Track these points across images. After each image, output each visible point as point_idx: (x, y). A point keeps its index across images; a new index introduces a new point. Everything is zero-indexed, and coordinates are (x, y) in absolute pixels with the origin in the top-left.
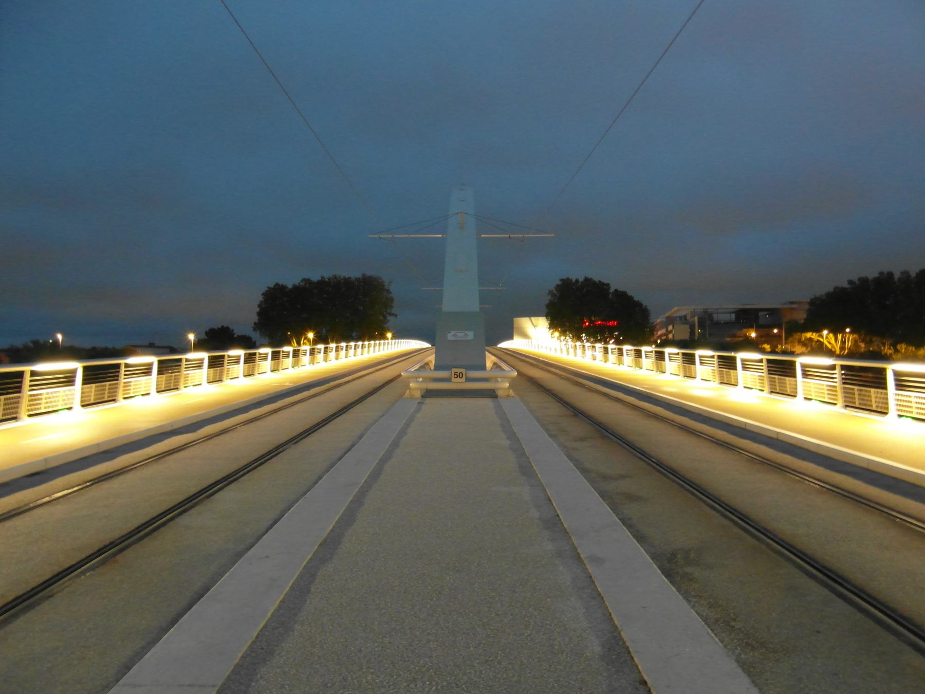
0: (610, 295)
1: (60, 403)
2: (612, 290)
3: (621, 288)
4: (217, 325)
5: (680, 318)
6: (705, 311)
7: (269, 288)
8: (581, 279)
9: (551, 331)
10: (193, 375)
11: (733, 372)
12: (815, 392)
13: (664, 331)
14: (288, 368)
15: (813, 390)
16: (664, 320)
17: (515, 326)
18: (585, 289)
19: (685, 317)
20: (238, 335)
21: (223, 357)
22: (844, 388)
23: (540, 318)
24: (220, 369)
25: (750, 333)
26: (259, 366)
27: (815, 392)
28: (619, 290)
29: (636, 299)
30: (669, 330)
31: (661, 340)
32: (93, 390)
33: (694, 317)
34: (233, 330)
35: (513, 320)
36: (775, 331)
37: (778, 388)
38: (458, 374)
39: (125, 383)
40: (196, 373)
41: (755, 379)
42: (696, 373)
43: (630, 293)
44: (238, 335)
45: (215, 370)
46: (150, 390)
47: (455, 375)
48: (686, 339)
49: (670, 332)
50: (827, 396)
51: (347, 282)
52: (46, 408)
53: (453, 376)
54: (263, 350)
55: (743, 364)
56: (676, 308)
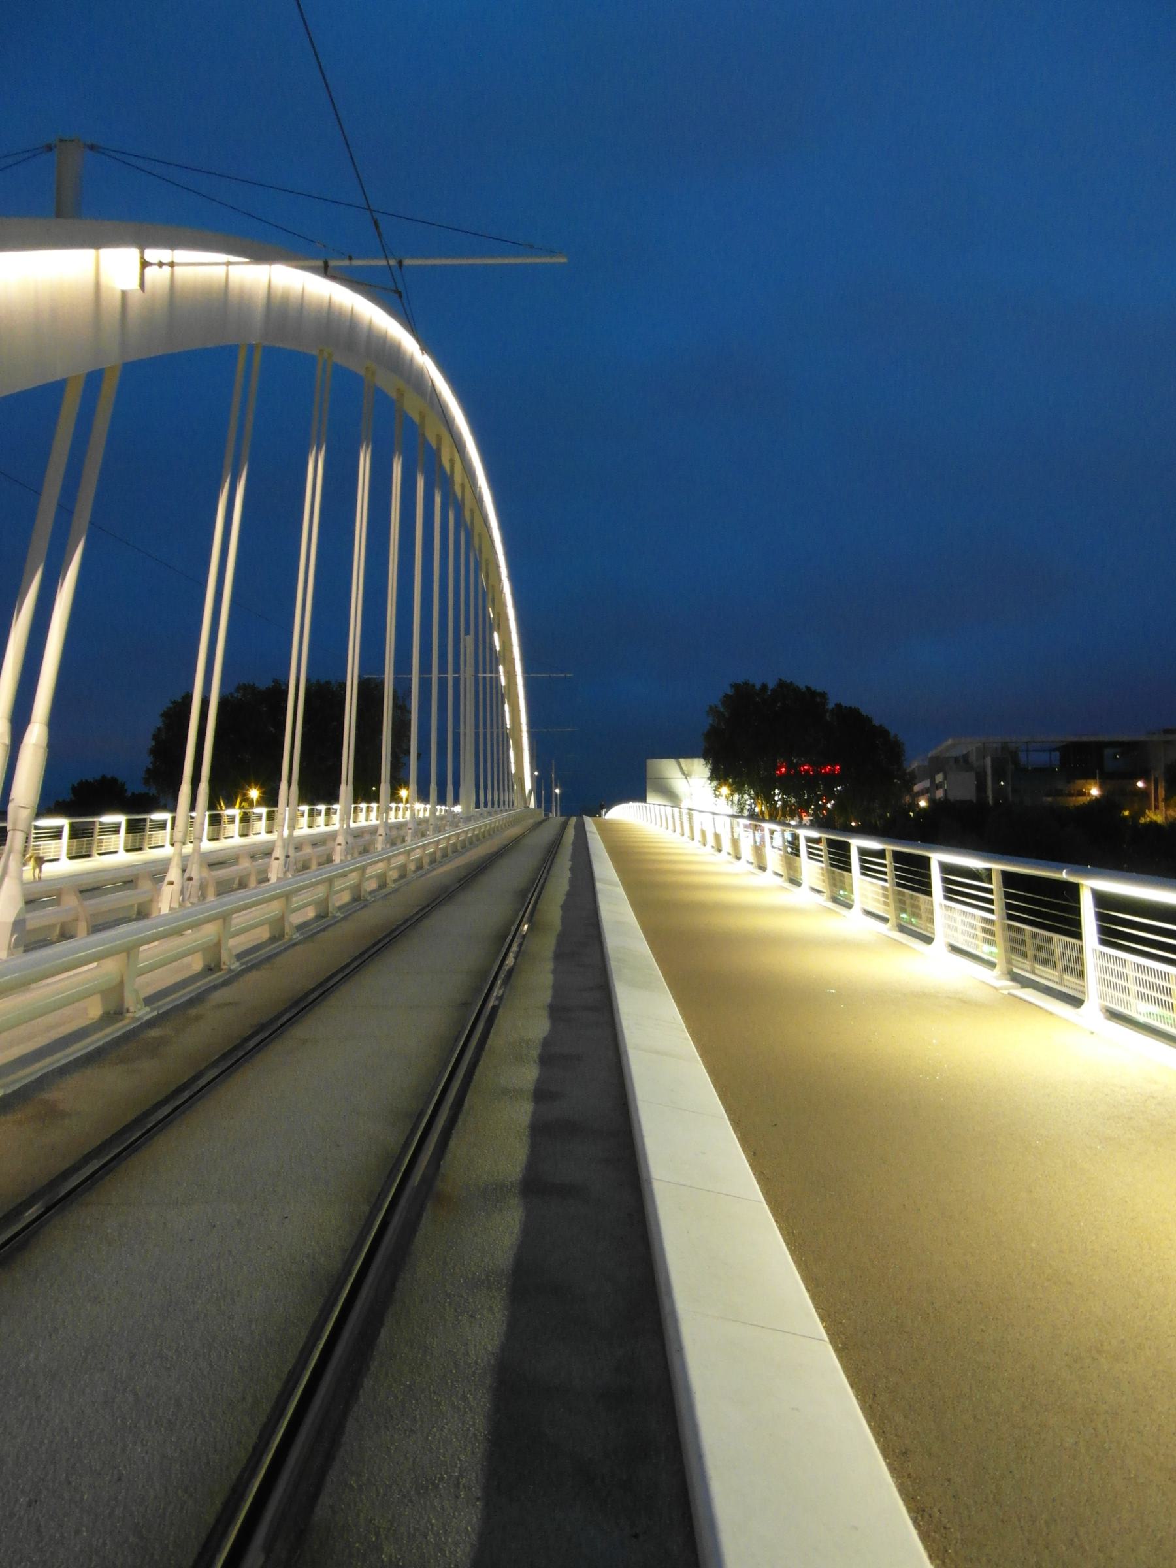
0: (828, 715)
1: (52, 854)
2: (831, 705)
3: (848, 702)
4: (92, 776)
5: (956, 760)
6: (1004, 747)
7: (173, 702)
8: (772, 685)
9: (715, 783)
10: (45, 851)
13: (926, 784)
14: (232, 837)
16: (926, 763)
17: (649, 774)
18: (779, 704)
19: (965, 758)
20: (133, 794)
21: (145, 820)
23: (696, 760)
24: (87, 840)
25: (1088, 787)
26: (225, 830)
28: (844, 704)
30: (937, 782)
31: (932, 801)
32: (75, 844)
33: (984, 758)
35: (646, 763)
36: (1140, 784)
39: (34, 846)
40: (111, 838)
45: (135, 836)
46: (118, 848)
48: (968, 798)
52: (105, 849)
54: (109, 819)
56: (950, 742)
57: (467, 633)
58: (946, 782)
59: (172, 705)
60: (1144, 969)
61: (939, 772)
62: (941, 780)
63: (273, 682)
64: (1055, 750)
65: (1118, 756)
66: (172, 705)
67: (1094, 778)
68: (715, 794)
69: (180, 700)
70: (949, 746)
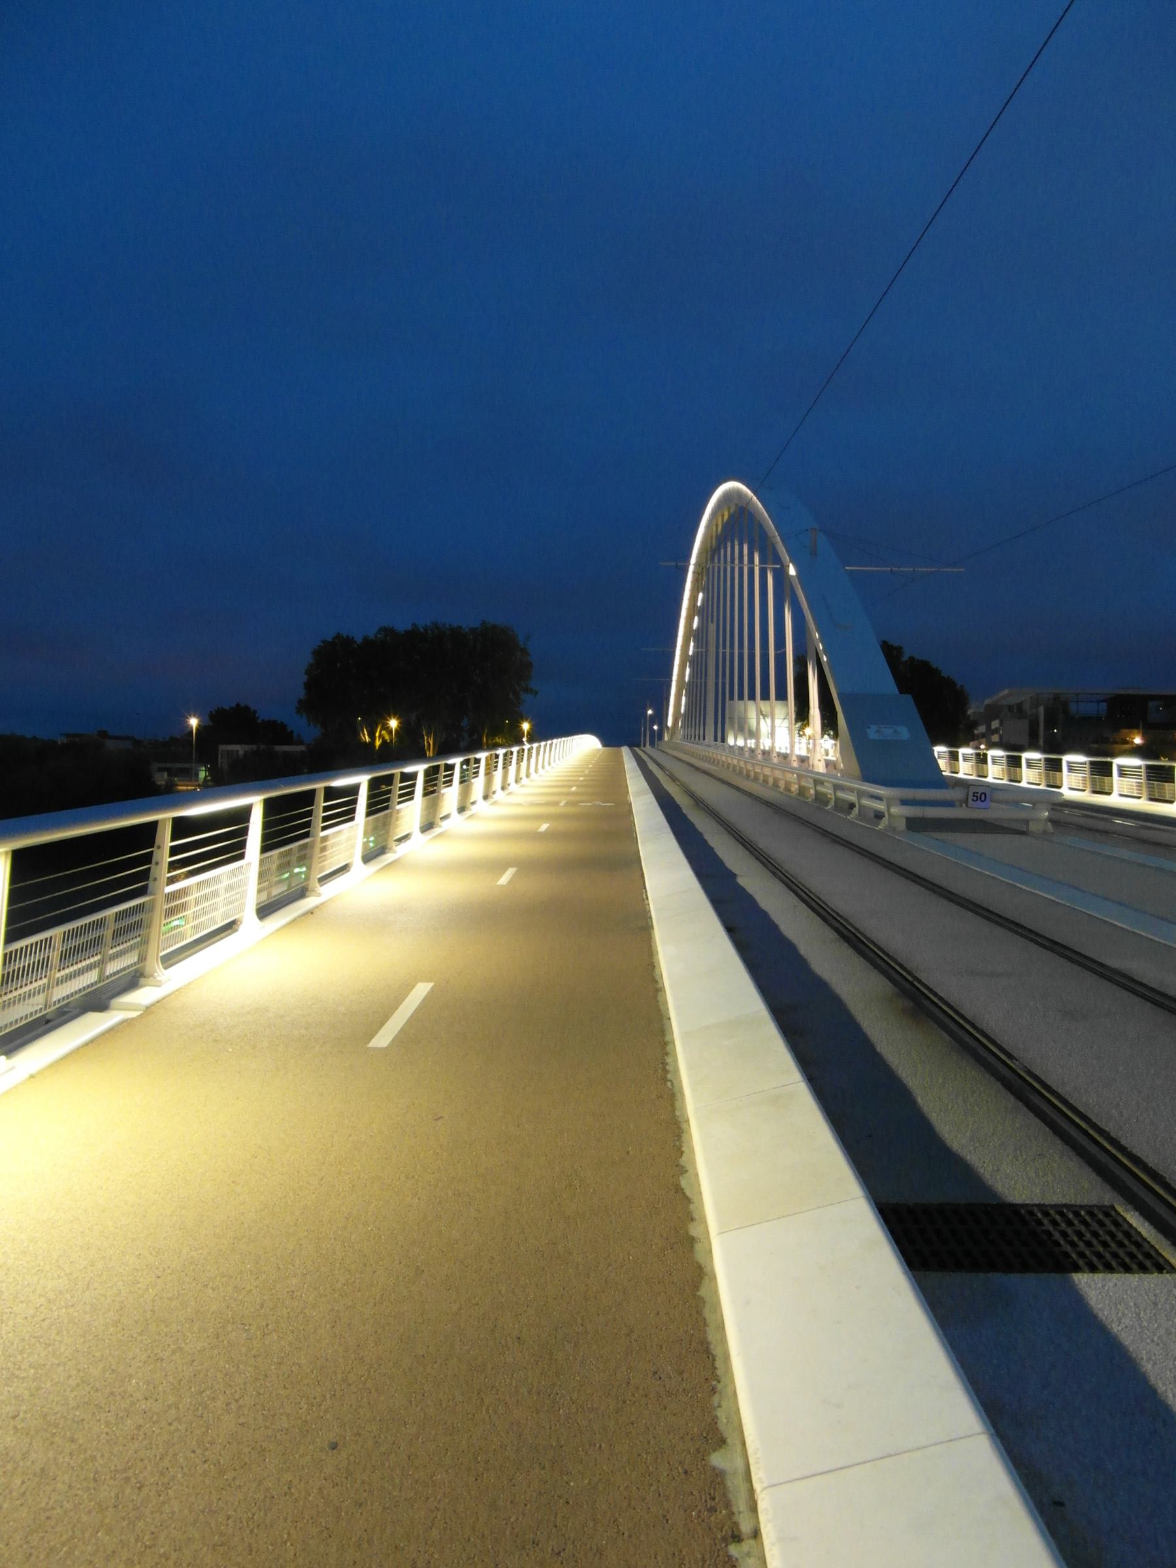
2: (905, 658)
5: (1010, 708)
6: (1056, 698)
9: (799, 724)
11: (1108, 779)
12: (1128, 788)
15: (1073, 781)
16: (982, 710)
19: (1020, 706)
20: (263, 720)
22: (1148, 784)
27: (1128, 788)
29: (944, 674)
30: (993, 727)
34: (255, 712)
37: (1157, 795)
38: (979, 795)
41: (1079, 780)
42: (1062, 781)
43: (935, 664)
44: (263, 720)
47: (974, 796)
49: (996, 731)
50: (1135, 791)
51: (456, 634)
53: (971, 797)
55: (1069, 766)
56: (1006, 692)
57: (712, 622)
58: (1001, 728)
59: (322, 644)
60: (1076, 776)
61: (996, 719)
62: (998, 726)
63: (412, 625)
64: (1104, 701)
65: (1161, 709)
66: (322, 644)
67: (1137, 727)
68: (799, 733)
69: (331, 640)
70: (1004, 696)
